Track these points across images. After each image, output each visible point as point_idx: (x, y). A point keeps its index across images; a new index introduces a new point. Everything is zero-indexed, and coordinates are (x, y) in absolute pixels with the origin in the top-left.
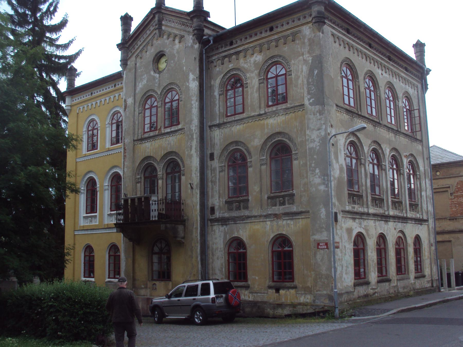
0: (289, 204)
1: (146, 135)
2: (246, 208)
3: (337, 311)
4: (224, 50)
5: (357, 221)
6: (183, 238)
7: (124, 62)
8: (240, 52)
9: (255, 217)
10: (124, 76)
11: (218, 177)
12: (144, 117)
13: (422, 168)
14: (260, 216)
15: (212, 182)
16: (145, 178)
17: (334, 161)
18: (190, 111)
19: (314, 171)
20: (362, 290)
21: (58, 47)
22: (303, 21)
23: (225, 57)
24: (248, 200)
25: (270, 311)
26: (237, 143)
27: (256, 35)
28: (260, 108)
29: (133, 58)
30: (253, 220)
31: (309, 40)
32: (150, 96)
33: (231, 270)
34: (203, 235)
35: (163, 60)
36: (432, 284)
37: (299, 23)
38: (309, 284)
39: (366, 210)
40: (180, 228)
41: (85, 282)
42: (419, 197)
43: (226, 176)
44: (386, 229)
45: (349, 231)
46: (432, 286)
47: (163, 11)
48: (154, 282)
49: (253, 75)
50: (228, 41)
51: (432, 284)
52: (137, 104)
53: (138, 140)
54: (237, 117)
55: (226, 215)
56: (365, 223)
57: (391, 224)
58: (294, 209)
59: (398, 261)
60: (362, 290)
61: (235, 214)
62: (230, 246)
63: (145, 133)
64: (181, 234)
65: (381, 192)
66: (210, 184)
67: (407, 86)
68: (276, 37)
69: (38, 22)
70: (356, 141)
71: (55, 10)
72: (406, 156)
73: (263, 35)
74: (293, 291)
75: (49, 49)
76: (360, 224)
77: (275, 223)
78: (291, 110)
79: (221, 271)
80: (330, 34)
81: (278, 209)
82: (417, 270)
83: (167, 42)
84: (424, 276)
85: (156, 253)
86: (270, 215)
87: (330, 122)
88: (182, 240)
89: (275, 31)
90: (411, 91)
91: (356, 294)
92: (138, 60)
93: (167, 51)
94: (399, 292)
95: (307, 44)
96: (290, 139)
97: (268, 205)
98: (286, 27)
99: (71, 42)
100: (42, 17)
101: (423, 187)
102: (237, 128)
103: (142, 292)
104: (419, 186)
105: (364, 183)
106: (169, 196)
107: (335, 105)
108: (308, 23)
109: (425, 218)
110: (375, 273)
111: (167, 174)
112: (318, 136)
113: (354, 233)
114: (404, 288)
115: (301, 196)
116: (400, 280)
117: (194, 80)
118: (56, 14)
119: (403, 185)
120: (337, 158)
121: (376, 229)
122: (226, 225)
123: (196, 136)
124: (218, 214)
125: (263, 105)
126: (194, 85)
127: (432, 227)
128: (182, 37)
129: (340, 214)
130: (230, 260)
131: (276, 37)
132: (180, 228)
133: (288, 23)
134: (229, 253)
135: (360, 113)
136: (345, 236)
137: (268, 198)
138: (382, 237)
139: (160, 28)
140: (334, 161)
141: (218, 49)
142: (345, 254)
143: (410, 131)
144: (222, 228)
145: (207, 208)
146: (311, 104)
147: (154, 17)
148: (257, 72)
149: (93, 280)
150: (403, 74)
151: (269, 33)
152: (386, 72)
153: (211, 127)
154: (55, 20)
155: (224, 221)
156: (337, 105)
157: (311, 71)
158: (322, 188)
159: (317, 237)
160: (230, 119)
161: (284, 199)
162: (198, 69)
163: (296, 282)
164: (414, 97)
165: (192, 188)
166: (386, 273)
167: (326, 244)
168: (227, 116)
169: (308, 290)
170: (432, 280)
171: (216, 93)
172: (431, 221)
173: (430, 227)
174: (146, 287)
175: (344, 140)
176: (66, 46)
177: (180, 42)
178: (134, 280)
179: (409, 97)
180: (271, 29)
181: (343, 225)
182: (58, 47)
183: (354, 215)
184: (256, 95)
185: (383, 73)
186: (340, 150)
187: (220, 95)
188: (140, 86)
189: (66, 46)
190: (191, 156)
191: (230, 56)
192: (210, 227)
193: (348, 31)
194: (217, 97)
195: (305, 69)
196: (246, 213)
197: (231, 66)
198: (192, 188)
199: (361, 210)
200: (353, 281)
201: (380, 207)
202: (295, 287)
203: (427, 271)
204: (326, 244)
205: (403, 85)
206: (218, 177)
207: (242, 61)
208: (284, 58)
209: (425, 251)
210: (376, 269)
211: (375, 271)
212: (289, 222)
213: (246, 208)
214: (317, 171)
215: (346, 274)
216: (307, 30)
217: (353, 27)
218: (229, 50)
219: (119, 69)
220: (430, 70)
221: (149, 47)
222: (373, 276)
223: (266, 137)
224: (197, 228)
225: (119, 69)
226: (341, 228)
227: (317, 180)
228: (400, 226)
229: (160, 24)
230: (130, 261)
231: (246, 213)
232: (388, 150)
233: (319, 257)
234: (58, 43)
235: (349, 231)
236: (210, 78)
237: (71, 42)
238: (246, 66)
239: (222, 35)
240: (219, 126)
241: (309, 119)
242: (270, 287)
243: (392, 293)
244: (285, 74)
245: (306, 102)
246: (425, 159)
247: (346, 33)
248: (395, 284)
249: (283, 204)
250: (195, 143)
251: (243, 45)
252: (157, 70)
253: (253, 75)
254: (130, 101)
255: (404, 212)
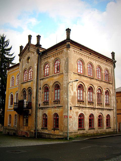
0: (59, 104)
1: (24, 82)
2: (48, 105)
3: (68, 138)
4: (45, 56)
5: (81, 109)
6: (31, 113)
7: (20, 60)
8: (48, 57)
9: (50, 107)
10: (20, 64)
11: (41, 95)
12: (24, 76)
13: (112, 93)
14: (51, 107)
15: (40, 96)
16: (24, 95)
17: (71, 91)
18: (35, 75)
19: (65, 94)
20: (81, 132)
21: (9, 55)
22: (64, 47)
23: (45, 58)
24: (48, 102)
25: (52, 137)
26: (46, 84)
27: (53, 51)
28: (53, 74)
29: (22, 59)
30: (49, 108)
31: (65, 53)
32: (26, 70)
33: (44, 123)
34: (36, 112)
35: (30, 59)
36: (114, 130)
37: (63, 48)
38: (62, 129)
39: (85, 106)
40: (30, 110)
41: (9, 126)
42: (110, 102)
43: (44, 95)
44: (94, 112)
45: (77, 113)
46: (114, 131)
47: (30, 45)
48: (24, 126)
49: (51, 64)
50: (46, 54)
51: (114, 130)
52: (23, 72)
53: (22, 83)
54: (47, 77)
55: (43, 107)
56: (84, 110)
57: (96, 111)
58: (60, 105)
59: (107, 123)
60: (81, 132)
61: (45, 106)
62: (43, 116)
63: (24, 81)
64: (30, 112)
65: (93, 100)
66: (39, 97)
67: (107, 66)
68: (57, 52)
69: (3, 48)
70: (82, 84)
71: (8, 44)
72: (105, 89)
73: (54, 52)
74: (58, 131)
75: (7, 56)
76: (82, 110)
77: (54, 109)
78: (60, 75)
79: (41, 124)
80: (73, 51)
81: (56, 105)
82: (107, 125)
83: (31, 54)
84: (111, 128)
85: (25, 118)
86: (54, 107)
87: (70, 78)
88: (31, 114)
89: (58, 50)
90: (108, 68)
91: (78, 133)
92: (24, 59)
93: (30, 57)
94: (98, 133)
95: (65, 54)
96: (60, 84)
97: (53, 104)
98: (60, 49)
99: (13, 54)
100: (5, 46)
101: (112, 99)
102: (47, 80)
103: (21, 129)
104: (110, 98)
105: (85, 97)
106: (29, 101)
107: (73, 73)
108: (65, 48)
109: (112, 109)
110: (88, 126)
111: (29, 94)
112: (66, 83)
113: (79, 114)
114: (101, 131)
115: (61, 102)
116: (99, 129)
117: (36, 65)
118: (8, 45)
119: (103, 98)
120: (72, 89)
121: (89, 112)
122: (43, 110)
123: (35, 82)
124: (41, 106)
125: (53, 73)
126: (36, 67)
127: (115, 112)
128: (34, 52)
129: (73, 107)
130: (44, 121)
131: (57, 52)
132: (30, 110)
133: (61, 48)
134: (43, 118)
135: (84, 75)
136: (75, 114)
137: (54, 102)
138: (91, 116)
139: (29, 50)
140: (71, 91)
141: (43, 56)
142: (75, 120)
143: (107, 80)
144: (42, 111)
145: (38, 104)
146: (65, 73)
147: (27, 47)
148: (52, 63)
149: (11, 125)
150: (105, 63)
151: (56, 51)
152: (97, 62)
153: (40, 80)
154: (9, 47)
155: (42, 108)
156: (74, 73)
157: (65, 63)
158: (67, 99)
159: (65, 114)
160: (46, 77)
161: (57, 102)
162: (37, 62)
163: (59, 128)
164: (110, 70)
165: (34, 98)
166: (93, 126)
167: (67, 117)
168: (45, 76)
169: (62, 131)
170: (114, 129)
171: (42, 70)
172: (115, 110)
173: (114, 112)
174: (22, 128)
175: (77, 84)
176: (12, 55)
177: (33, 54)
178: (19, 126)
179: (107, 70)
180: (56, 50)
181: (74, 111)
182: (9, 55)
183: (79, 107)
184: (52, 70)
185: (96, 62)
186: (75, 87)
187: (43, 70)
188: (23, 67)
189: (12, 55)
190: (34, 88)
191: (46, 58)
192: (38, 110)
193: (81, 50)
194: (42, 70)
195: (64, 62)
196: (48, 106)
197: (46, 61)
198: (34, 98)
199: (83, 106)
200: (78, 129)
201: (92, 105)
202: (59, 130)
203: (112, 126)
204: (67, 117)
205: (105, 66)
206: (41, 95)
207: (49, 59)
208: (59, 59)
209: (111, 119)
210: (88, 125)
211: (88, 125)
212: (58, 109)
213: (48, 105)
214: (66, 94)
215: (75, 126)
216: (65, 50)
217: (83, 48)
218: (46, 56)
219: (19, 62)
220: (116, 61)
221: (26, 56)
222: (87, 127)
223: (54, 83)
224: (34, 110)
225: (19, 62)
226: (73, 112)
227: (66, 97)
228: (100, 111)
229: (29, 49)
230: (19, 120)
231: (48, 106)
232: (96, 87)
233: (65, 120)
234: (10, 54)
235: (77, 113)
236: (41, 65)
237: (13, 54)
238: (50, 61)
239: (45, 51)
240: (42, 79)
241: (64, 77)
242: (52, 129)
243: (95, 133)
244: (59, 64)
245: (64, 72)
246: (113, 90)
247: (80, 50)
248: (97, 130)
249: (57, 104)
250: (35, 85)
251: (49, 55)
252: (28, 62)
253: (51, 64)
254: (21, 71)
255: (103, 107)
